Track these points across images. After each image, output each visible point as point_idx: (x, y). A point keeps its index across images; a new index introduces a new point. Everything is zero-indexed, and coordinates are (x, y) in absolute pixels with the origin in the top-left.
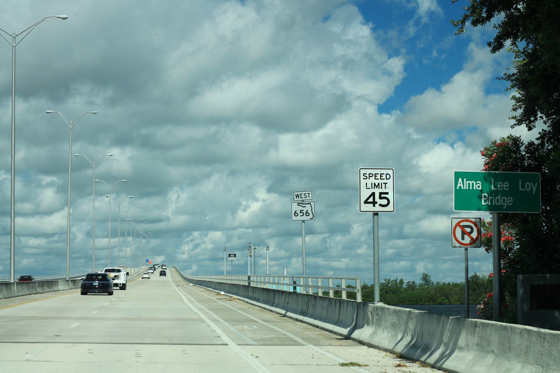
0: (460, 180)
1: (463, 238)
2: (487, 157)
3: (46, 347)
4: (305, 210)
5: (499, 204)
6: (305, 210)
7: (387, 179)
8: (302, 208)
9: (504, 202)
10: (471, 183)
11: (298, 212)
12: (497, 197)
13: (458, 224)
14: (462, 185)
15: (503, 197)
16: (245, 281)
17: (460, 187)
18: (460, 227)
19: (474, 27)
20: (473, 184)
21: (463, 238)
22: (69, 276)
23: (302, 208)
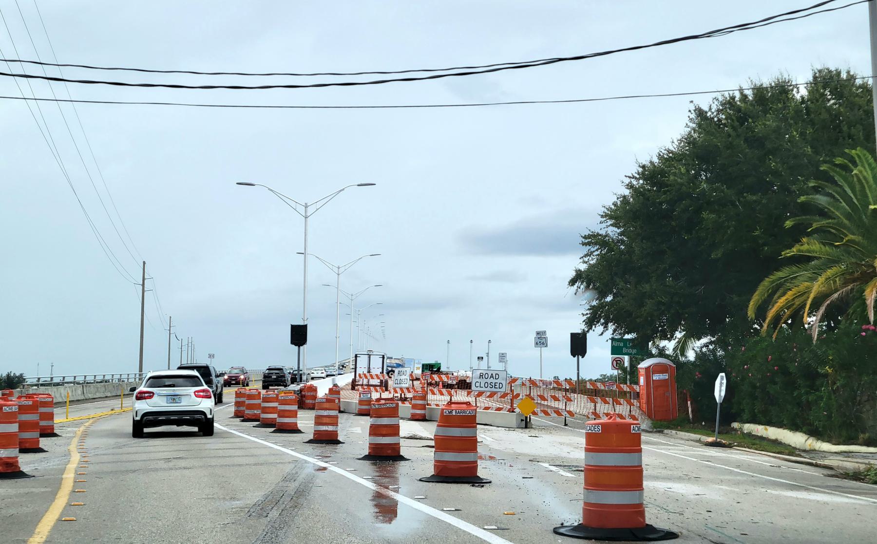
1: (617, 366)
7: (499, 388)
13: (614, 360)
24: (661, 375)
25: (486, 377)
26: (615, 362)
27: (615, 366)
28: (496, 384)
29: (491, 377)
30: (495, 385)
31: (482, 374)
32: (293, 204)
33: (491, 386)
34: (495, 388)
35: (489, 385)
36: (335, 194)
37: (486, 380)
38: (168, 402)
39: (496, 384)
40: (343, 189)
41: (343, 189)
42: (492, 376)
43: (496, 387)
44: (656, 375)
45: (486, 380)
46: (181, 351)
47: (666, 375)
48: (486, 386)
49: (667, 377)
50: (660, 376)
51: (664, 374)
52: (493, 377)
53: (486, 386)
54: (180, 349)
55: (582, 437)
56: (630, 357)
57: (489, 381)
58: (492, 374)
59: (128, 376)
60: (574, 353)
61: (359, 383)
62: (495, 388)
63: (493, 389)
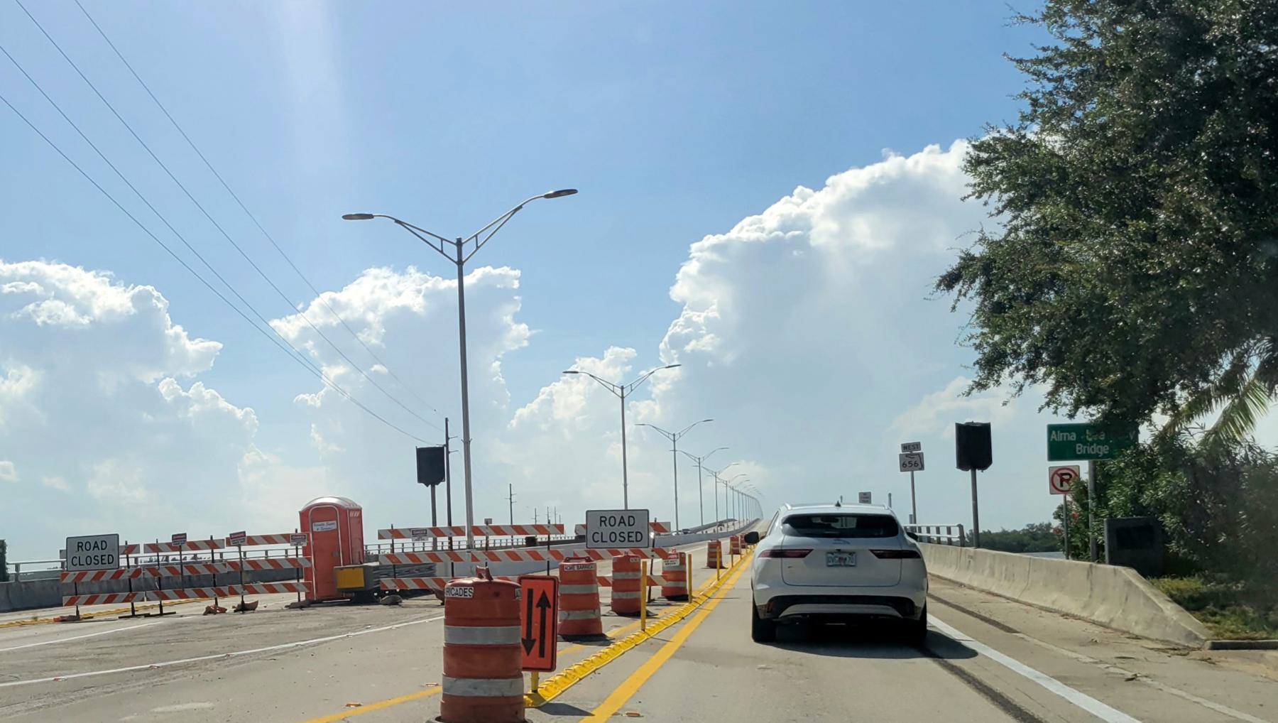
0: (1054, 432)
1: (1062, 485)
2: (1220, 383)
3: (972, 639)
4: (913, 461)
5: (1094, 453)
6: (913, 461)
7: (109, 563)
8: (910, 460)
9: (1100, 451)
10: (1065, 434)
11: (907, 463)
12: (1092, 447)
13: (1056, 473)
14: (1055, 437)
15: (1099, 446)
16: (494, 543)
17: (1054, 439)
18: (1058, 475)
19: (212, 538)
20: (1067, 436)
21: (1062, 485)
22: (950, 542)
23: (910, 460)
24: (325, 523)
25: (612, 524)
26: (1057, 479)
27: (1058, 485)
28: (103, 558)
29: (620, 522)
30: (629, 537)
31: (80, 545)
32: (437, 243)
33: (622, 539)
34: (629, 541)
35: (618, 538)
36: (509, 215)
37: (613, 529)
38: (830, 564)
39: (631, 534)
40: (521, 207)
41: (521, 207)
42: (96, 546)
43: (631, 539)
44: (317, 523)
45: (613, 529)
46: (511, 503)
47: (333, 524)
48: (89, 563)
49: (334, 527)
50: (323, 525)
51: (330, 522)
52: (624, 523)
53: (613, 539)
54: (509, 501)
55: (760, 606)
56: (1095, 463)
57: (617, 529)
58: (622, 517)
59: (403, 545)
60: (904, 467)
61: (484, 542)
62: (629, 541)
63: (100, 566)
